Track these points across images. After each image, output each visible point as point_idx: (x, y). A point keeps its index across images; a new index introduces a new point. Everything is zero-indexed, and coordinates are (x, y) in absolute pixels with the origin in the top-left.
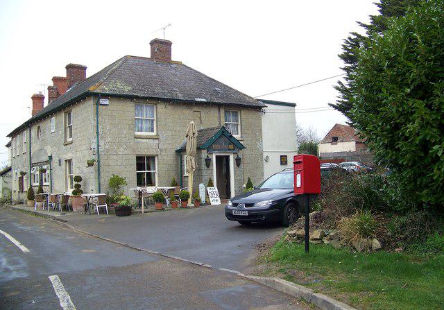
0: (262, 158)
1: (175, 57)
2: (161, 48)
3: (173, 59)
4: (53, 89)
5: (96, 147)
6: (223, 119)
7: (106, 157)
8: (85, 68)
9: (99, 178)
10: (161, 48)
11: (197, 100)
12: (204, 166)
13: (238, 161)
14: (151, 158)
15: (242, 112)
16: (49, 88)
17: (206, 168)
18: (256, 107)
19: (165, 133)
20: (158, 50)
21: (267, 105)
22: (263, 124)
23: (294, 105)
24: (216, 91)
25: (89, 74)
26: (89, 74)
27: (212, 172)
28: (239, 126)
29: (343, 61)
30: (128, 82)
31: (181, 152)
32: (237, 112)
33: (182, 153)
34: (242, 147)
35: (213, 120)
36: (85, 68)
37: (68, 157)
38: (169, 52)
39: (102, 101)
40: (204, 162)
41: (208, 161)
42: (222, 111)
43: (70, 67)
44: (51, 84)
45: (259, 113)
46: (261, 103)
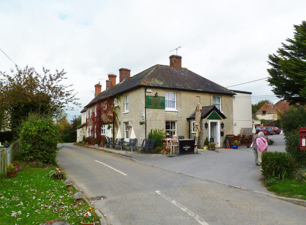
0: (233, 124)
1: (184, 65)
2: (176, 60)
3: (182, 67)
4: (109, 81)
5: (145, 116)
6: (212, 101)
7: (149, 121)
8: (129, 71)
9: (146, 134)
10: (176, 60)
11: (198, 90)
12: (204, 128)
13: (222, 125)
14: (173, 123)
15: (222, 98)
16: (107, 81)
17: (205, 129)
18: (230, 94)
19: (178, 107)
20: (175, 61)
21: (236, 93)
22: (233, 104)
23: (250, 93)
24: (207, 85)
25: (132, 74)
26: (132, 74)
27: (208, 131)
28: (220, 106)
29: (268, 73)
30: (160, 80)
31: (192, 118)
32: (219, 97)
33: (190, 120)
34: (224, 117)
35: (207, 101)
36: (129, 71)
37: (126, 120)
38: (180, 62)
39: (148, 90)
40: (204, 126)
41: (206, 125)
42: (212, 97)
43: (171, 57)
44: (108, 79)
45: (231, 98)
46: (233, 92)
